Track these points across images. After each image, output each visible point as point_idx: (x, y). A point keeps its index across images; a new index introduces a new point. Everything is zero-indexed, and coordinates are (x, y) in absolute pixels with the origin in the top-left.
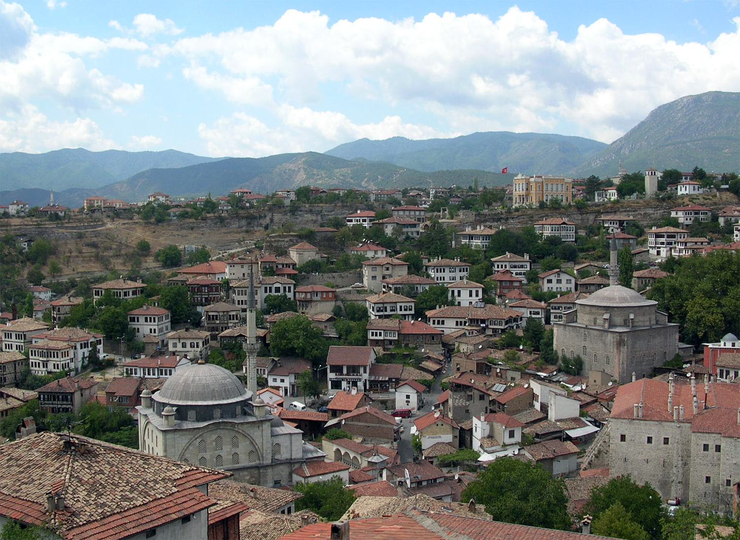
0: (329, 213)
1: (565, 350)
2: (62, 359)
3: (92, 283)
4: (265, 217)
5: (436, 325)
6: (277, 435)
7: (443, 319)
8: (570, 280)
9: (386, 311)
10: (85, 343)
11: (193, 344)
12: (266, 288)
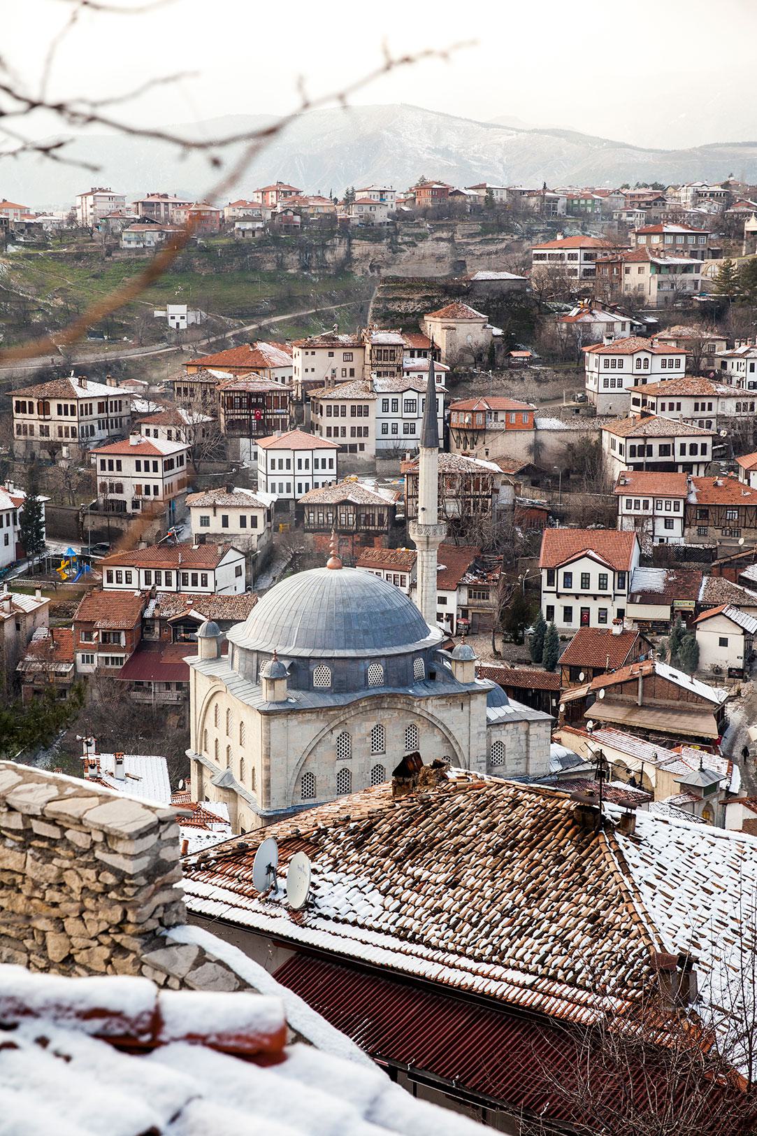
0: (469, 240)
9: (650, 454)
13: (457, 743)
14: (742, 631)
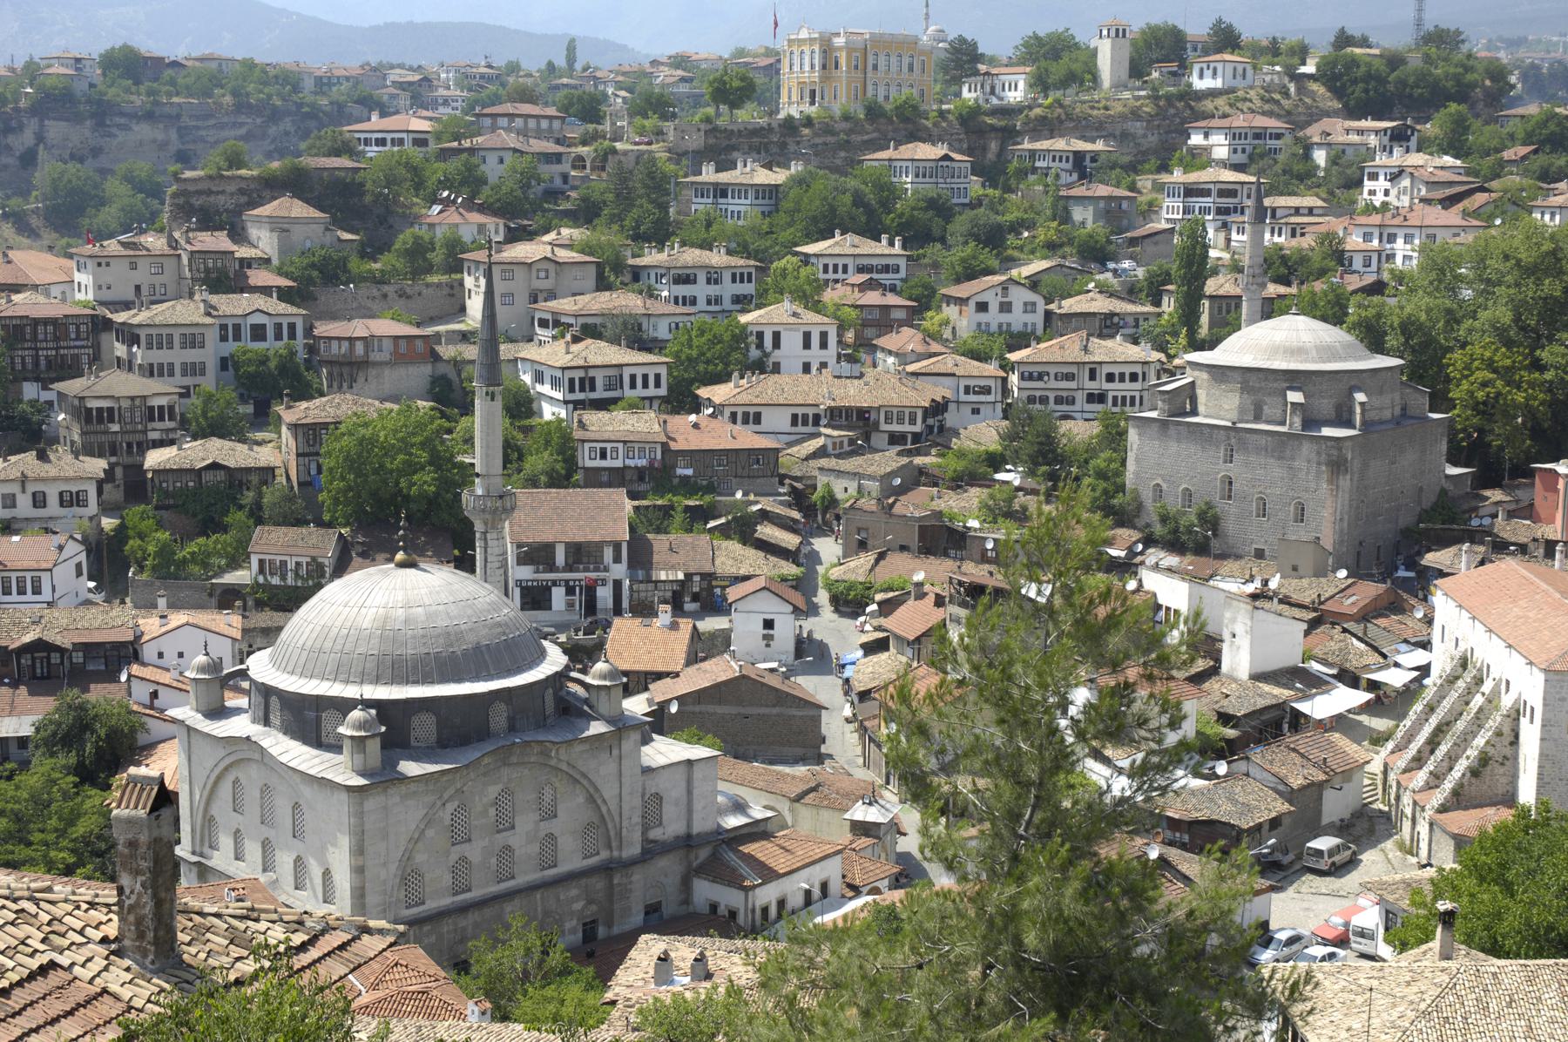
0: (200, 123)
1: (1164, 486)
4: (21, 128)
8: (1034, 304)
9: (593, 389)
13: (604, 801)
14: (790, 608)
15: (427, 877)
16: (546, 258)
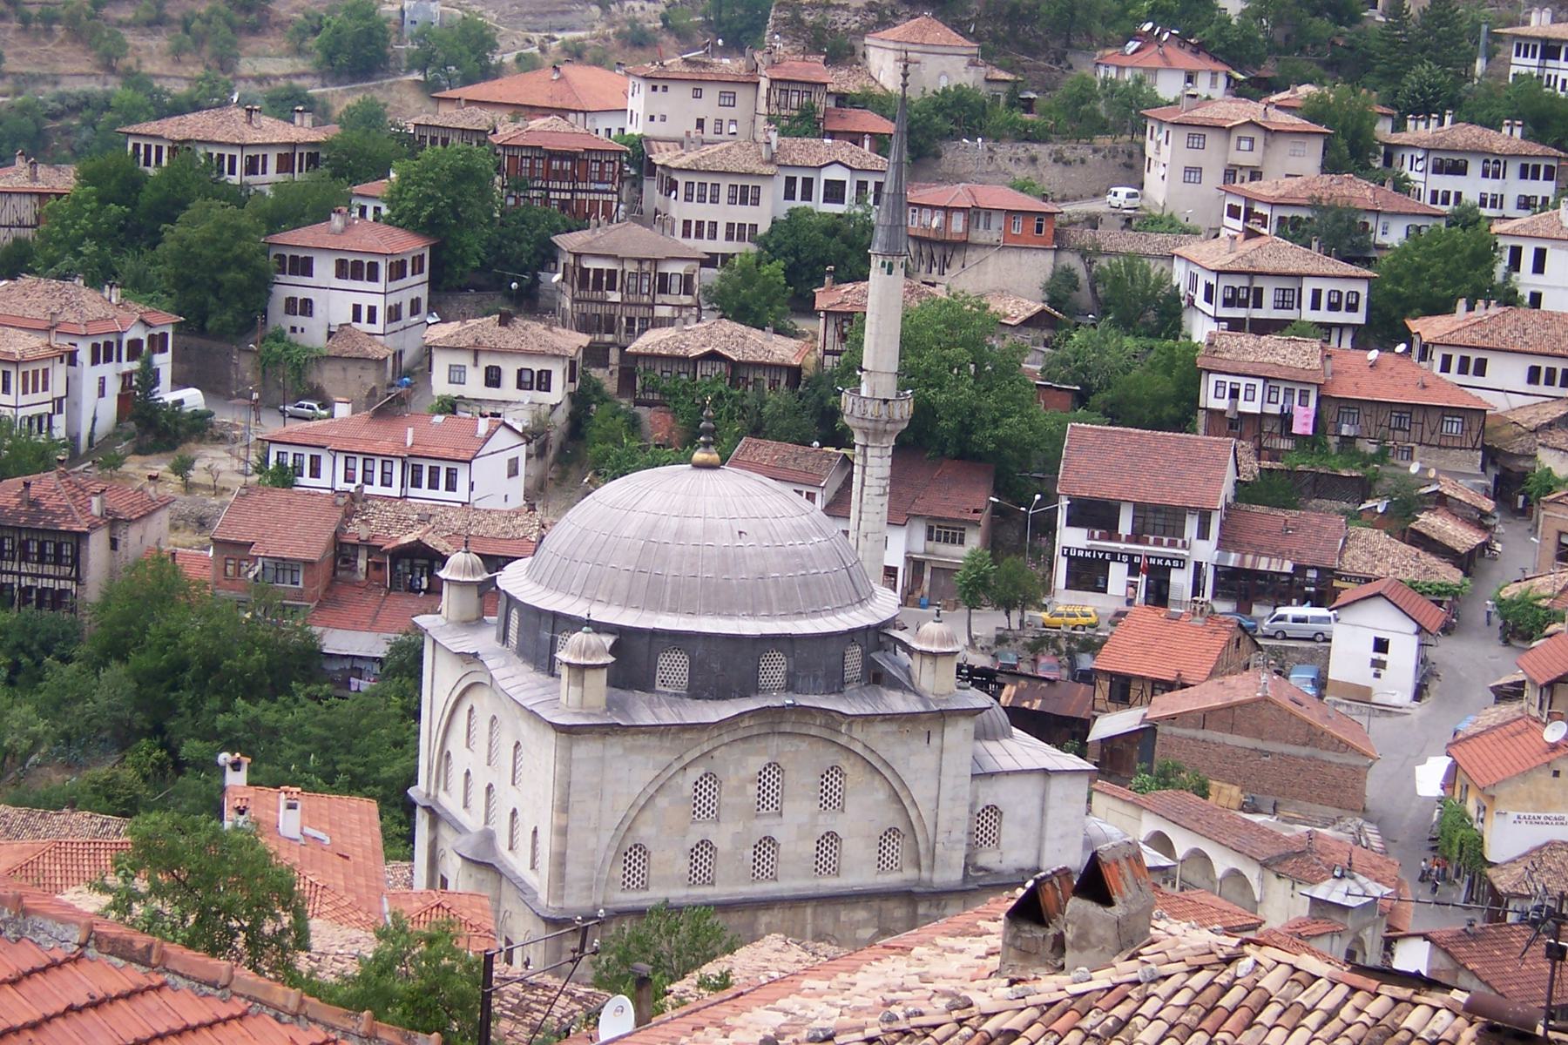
2: (23, 400)
3: (55, 116)
5: (1453, 376)
6: (992, 774)
7: (1482, 355)
9: (1258, 304)
10: (108, 345)
11: (527, 377)
12: (791, 182)
15: (655, 857)
16: (1251, 123)
